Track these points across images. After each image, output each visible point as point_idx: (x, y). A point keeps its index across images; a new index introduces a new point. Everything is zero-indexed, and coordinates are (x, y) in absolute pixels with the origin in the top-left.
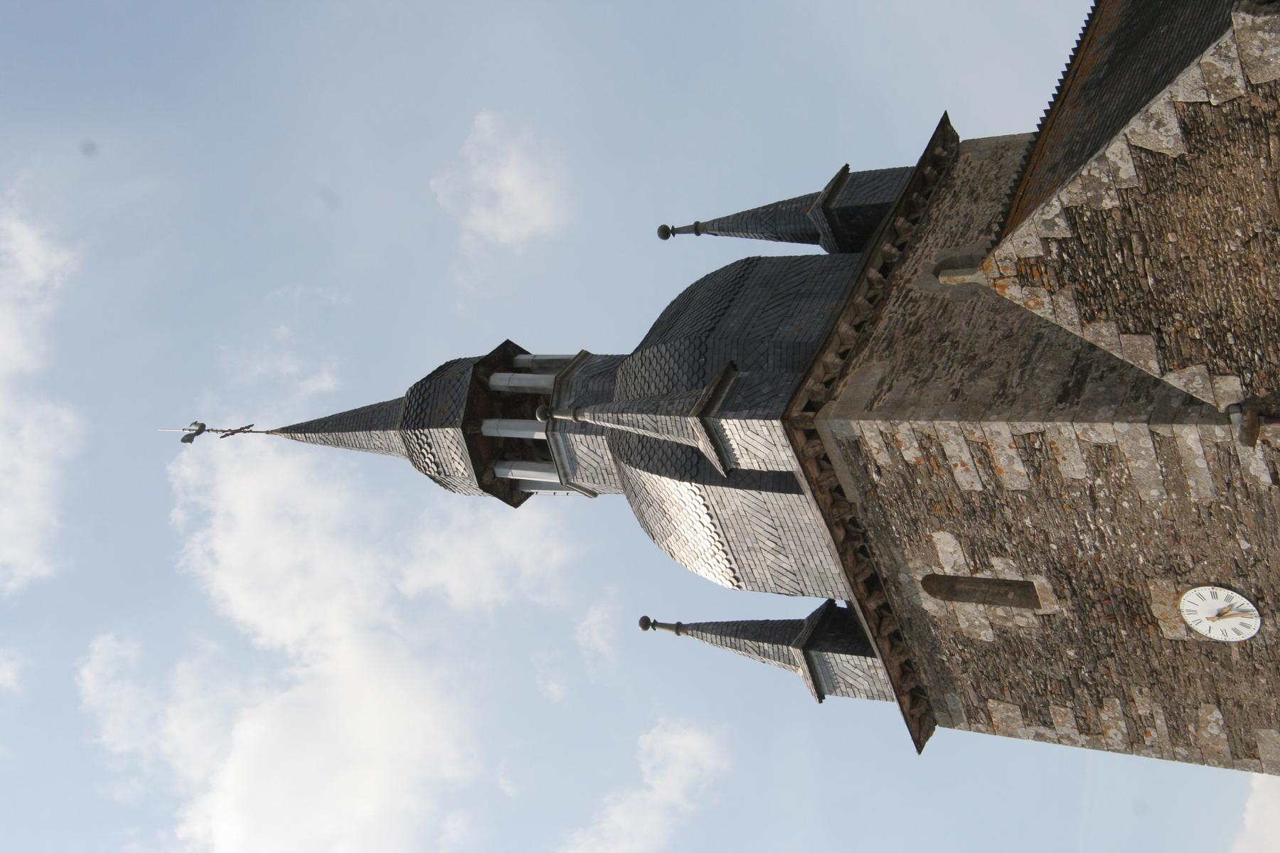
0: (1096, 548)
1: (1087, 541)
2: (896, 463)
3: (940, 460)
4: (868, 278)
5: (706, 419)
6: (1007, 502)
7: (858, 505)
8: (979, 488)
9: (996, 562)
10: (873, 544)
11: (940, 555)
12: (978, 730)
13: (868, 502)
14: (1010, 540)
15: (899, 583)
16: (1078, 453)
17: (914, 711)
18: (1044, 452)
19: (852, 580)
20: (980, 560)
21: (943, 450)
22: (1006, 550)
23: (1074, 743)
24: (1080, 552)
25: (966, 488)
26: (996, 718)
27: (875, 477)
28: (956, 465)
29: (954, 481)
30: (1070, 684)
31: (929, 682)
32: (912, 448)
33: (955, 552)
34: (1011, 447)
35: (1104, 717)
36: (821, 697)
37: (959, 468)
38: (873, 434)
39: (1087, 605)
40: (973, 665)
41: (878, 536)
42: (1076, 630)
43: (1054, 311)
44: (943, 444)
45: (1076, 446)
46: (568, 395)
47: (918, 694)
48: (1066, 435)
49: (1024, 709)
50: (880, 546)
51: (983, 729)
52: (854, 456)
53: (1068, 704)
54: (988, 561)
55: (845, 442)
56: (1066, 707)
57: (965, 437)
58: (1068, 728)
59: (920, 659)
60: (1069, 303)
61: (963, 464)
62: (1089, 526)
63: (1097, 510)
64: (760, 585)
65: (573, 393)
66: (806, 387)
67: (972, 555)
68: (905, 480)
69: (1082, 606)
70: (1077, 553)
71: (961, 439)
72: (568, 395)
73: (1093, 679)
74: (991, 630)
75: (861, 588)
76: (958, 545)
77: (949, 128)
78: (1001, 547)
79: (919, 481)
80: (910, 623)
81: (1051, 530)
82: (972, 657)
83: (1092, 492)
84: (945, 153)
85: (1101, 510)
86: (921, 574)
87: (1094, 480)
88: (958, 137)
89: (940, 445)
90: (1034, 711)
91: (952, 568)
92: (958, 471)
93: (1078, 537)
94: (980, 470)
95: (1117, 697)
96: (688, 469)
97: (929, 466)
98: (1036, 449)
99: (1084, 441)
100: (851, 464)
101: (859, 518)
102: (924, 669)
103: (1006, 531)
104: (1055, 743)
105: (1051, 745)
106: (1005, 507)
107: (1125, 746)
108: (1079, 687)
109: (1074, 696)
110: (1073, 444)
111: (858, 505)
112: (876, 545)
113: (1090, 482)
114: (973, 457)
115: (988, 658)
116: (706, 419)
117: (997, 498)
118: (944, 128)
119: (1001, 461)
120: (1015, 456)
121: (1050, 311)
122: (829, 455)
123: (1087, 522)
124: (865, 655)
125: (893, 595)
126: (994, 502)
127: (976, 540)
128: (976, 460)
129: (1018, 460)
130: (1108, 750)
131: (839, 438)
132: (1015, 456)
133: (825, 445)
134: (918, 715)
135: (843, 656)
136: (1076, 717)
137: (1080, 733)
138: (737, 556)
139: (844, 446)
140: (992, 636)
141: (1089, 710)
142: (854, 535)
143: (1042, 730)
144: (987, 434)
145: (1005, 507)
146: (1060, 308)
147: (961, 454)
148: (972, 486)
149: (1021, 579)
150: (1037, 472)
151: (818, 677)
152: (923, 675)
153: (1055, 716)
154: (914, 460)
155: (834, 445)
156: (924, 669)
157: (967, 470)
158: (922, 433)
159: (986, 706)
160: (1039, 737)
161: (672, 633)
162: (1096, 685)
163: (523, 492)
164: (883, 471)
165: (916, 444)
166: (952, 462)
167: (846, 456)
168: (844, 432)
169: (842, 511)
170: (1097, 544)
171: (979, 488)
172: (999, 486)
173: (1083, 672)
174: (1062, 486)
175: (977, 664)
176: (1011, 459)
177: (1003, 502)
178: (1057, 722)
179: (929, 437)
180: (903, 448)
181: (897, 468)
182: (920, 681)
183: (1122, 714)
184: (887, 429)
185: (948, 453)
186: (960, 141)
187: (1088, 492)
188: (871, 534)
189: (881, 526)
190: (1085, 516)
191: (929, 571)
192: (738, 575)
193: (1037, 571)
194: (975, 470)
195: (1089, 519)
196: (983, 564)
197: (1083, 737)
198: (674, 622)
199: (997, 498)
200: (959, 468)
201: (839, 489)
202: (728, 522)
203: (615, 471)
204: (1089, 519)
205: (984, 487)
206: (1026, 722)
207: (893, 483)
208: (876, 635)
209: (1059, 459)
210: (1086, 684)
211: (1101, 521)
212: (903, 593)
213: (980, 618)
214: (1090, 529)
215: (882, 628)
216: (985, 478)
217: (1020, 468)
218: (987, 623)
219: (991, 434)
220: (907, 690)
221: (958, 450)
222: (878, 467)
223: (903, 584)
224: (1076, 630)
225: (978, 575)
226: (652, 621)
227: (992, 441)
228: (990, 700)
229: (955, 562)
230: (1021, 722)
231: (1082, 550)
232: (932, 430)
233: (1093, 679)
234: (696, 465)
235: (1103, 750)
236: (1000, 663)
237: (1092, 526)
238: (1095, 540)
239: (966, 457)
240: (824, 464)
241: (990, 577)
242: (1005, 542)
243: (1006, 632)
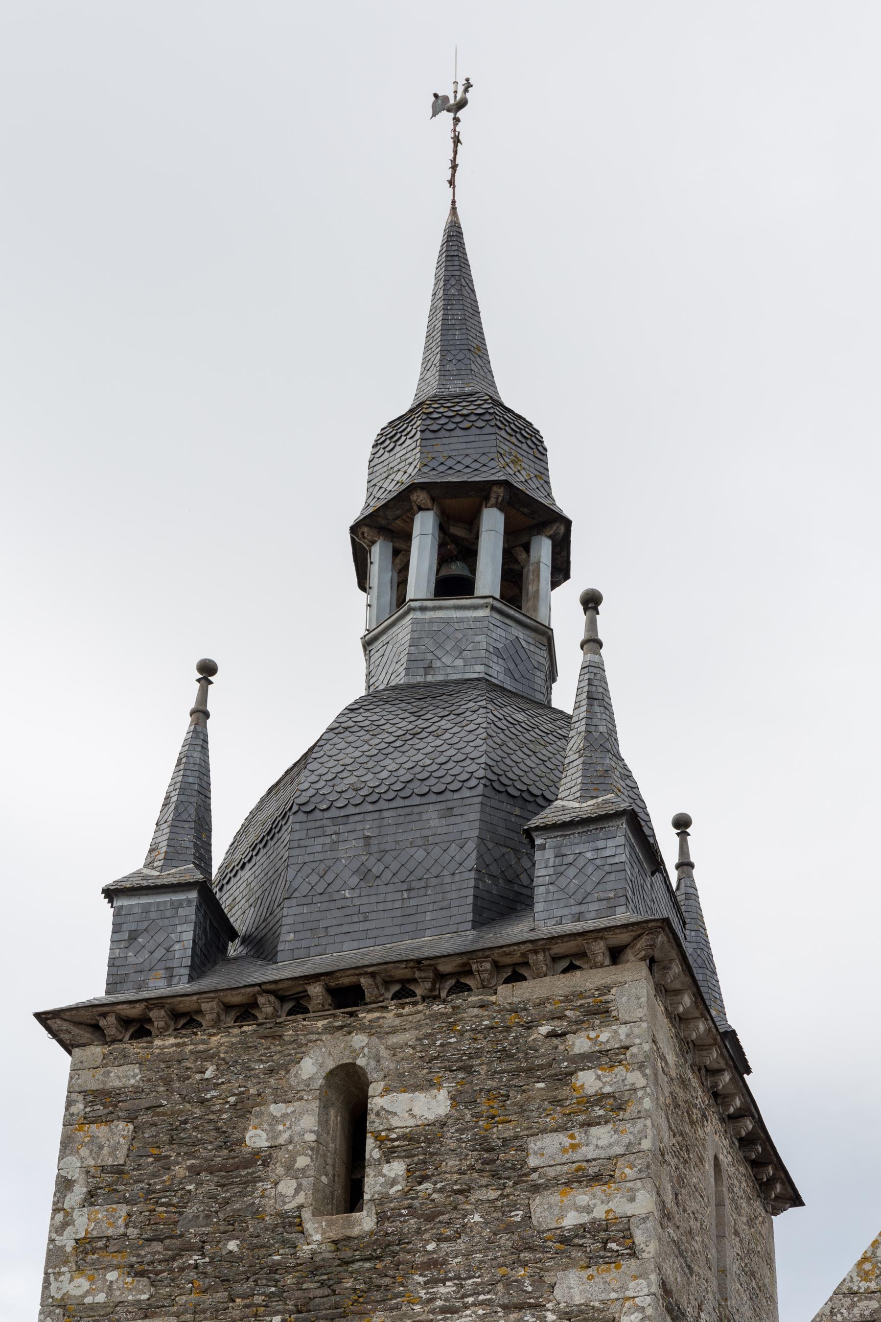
0: (430, 1301)
1: (443, 1290)
2: (573, 1059)
3: (582, 1118)
4: (724, 1070)
5: (624, 820)
6: (507, 1196)
7: (493, 998)
8: (533, 1162)
9: (397, 1168)
10: (420, 1007)
11: (406, 1095)
12: (69, 1103)
13: (499, 1011)
14: (441, 1191)
15: (350, 1033)
16: (604, 1296)
17: (111, 1019)
18: (602, 1253)
19: (370, 970)
20: (398, 1146)
21: (599, 1124)
22: (420, 1183)
23: (58, 1229)
24: (421, 1279)
25: (532, 1145)
26: (100, 1131)
27: (544, 1030)
28: (572, 1137)
29: (544, 1131)
30: (170, 1237)
31: (162, 1048)
32: (601, 1085)
33: (414, 1116)
34: (607, 1212)
35: (112, 1276)
36: (110, 893)
37: (567, 1142)
38: (623, 1037)
39: (325, 1277)
40: (198, 1112)
41: (435, 1017)
42: (278, 1258)
43: (855, 1293)
44: (610, 1126)
45: (613, 1295)
46: (530, 640)
47: (131, 1030)
48: (632, 1285)
49: (119, 1171)
50: (419, 1016)
51: (73, 1109)
52: (582, 1006)
53: (133, 1232)
54: (398, 1157)
55: (609, 997)
56: (127, 1226)
57: (623, 1155)
58: (82, 1224)
59: (203, 1042)
60: (867, 1313)
61: (574, 1147)
62: (470, 1296)
63: (500, 1310)
64: (302, 843)
65: (532, 648)
66: (677, 961)
67: (409, 1138)
68: (541, 1067)
69: (323, 1270)
70: (421, 1275)
71: (619, 1150)
72: (530, 640)
73: (182, 1269)
74: (267, 1144)
75: (345, 981)
76: (426, 1122)
77: (788, 1205)
78: (423, 1179)
79: (541, 1085)
80: (274, 1037)
81: (461, 1245)
82: (213, 1112)
83: (531, 1306)
84: (773, 1196)
85: (500, 1314)
86: (368, 1064)
87: (553, 1311)
88: (776, 1214)
89: (606, 1122)
90: (115, 1183)
91: (383, 1108)
92: (563, 1139)
93: (450, 1279)
94: (566, 1167)
95: (152, 1296)
96: (507, 773)
97: (568, 1102)
98: (606, 1243)
99: (622, 1305)
100: (567, 999)
101: (469, 996)
102: (184, 1044)
103: (455, 1187)
104: (55, 1203)
105: (51, 1199)
106: (499, 1192)
107: (58, 1296)
108: (166, 1249)
109: (147, 1240)
110: (616, 1291)
111: (493, 998)
112: (420, 1012)
113: (549, 1306)
114: (587, 1161)
115: (213, 1133)
116: (624, 820)
117: (515, 1183)
118: (796, 1201)
119: (582, 1198)
120: (591, 1216)
121: (855, 1288)
122: (578, 973)
123: (479, 1294)
124: (192, 967)
125: (326, 1022)
126: (508, 1178)
127: (438, 1146)
128: (584, 1164)
129: (585, 1218)
130: (46, 1273)
131: (613, 991)
132: (591, 1216)
133: (600, 970)
134: (102, 1023)
135: (190, 936)
136: (108, 1238)
137: (77, 1241)
138: (352, 819)
139: (600, 995)
140: (258, 1145)
141: (123, 1257)
142: (437, 986)
143: (79, 1191)
144: (629, 1184)
145: (499, 1192)
146: (860, 1300)
147: (592, 1147)
148: (536, 1153)
149: (367, 1197)
150: (564, 1240)
151: (182, 891)
152: (172, 1041)
153: (107, 1211)
154: (578, 1084)
155: (599, 982)
156: (184, 1044)
157: (564, 1150)
158: (627, 1101)
159: (119, 1118)
160: (64, 1185)
161: (192, 704)
162: (171, 1271)
163: (373, 543)
164: (556, 1041)
165: (607, 1090)
166: (576, 1132)
167: (581, 995)
168: (624, 999)
169: (485, 975)
170: (439, 1303)
171: (533, 1162)
172: (536, 1189)
173: (196, 1257)
174: (541, 1269)
175: (200, 1118)
176: (588, 1209)
177: (507, 1191)
178: (97, 1212)
179: (620, 1108)
180: (599, 1072)
181: (564, 1060)
182: (162, 1034)
183: (119, 1299)
184: (632, 1055)
185: (594, 1130)
186: (772, 1217)
187: (532, 1301)
188: (438, 1008)
189: (455, 1023)
190: (488, 1293)
191: (373, 1075)
192: (318, 814)
193: (381, 1218)
194: (564, 1160)
195: (481, 1297)
196: (393, 1150)
197: (70, 1246)
198: (210, 708)
199: (515, 1183)
200: (567, 1142)
201: (516, 977)
202: (415, 817)
203: (429, 678)
204: (481, 1297)
205: (534, 1170)
206: (92, 1170)
207: (536, 1050)
208: (264, 987)
209: (590, 1271)
210: (173, 1259)
211: (481, 1312)
212: (329, 1037)
213: (288, 1133)
214: (464, 1296)
215: (272, 998)
216: (551, 1172)
217: (571, 1220)
218: (281, 1140)
219: (631, 1190)
220: (152, 1014)
221: (600, 1143)
222: (564, 1034)
223: (348, 1038)
224: (278, 1258)
225: (370, 1142)
226: (210, 678)
227: (618, 1189)
228: (131, 1127)
229: (395, 1114)
230: (92, 1163)
231: (426, 1283)
232: (635, 1115)
233: (182, 1269)
234: (506, 791)
235: (47, 1266)
236: (205, 1149)
237: (470, 1300)
238: (446, 1300)
239: (588, 1152)
240: (565, 964)
241: (367, 1156)
242: (435, 1184)
243: (265, 1164)
